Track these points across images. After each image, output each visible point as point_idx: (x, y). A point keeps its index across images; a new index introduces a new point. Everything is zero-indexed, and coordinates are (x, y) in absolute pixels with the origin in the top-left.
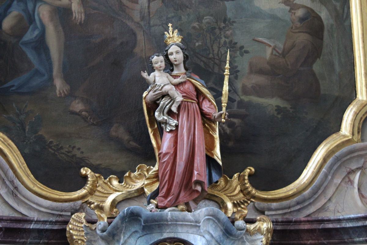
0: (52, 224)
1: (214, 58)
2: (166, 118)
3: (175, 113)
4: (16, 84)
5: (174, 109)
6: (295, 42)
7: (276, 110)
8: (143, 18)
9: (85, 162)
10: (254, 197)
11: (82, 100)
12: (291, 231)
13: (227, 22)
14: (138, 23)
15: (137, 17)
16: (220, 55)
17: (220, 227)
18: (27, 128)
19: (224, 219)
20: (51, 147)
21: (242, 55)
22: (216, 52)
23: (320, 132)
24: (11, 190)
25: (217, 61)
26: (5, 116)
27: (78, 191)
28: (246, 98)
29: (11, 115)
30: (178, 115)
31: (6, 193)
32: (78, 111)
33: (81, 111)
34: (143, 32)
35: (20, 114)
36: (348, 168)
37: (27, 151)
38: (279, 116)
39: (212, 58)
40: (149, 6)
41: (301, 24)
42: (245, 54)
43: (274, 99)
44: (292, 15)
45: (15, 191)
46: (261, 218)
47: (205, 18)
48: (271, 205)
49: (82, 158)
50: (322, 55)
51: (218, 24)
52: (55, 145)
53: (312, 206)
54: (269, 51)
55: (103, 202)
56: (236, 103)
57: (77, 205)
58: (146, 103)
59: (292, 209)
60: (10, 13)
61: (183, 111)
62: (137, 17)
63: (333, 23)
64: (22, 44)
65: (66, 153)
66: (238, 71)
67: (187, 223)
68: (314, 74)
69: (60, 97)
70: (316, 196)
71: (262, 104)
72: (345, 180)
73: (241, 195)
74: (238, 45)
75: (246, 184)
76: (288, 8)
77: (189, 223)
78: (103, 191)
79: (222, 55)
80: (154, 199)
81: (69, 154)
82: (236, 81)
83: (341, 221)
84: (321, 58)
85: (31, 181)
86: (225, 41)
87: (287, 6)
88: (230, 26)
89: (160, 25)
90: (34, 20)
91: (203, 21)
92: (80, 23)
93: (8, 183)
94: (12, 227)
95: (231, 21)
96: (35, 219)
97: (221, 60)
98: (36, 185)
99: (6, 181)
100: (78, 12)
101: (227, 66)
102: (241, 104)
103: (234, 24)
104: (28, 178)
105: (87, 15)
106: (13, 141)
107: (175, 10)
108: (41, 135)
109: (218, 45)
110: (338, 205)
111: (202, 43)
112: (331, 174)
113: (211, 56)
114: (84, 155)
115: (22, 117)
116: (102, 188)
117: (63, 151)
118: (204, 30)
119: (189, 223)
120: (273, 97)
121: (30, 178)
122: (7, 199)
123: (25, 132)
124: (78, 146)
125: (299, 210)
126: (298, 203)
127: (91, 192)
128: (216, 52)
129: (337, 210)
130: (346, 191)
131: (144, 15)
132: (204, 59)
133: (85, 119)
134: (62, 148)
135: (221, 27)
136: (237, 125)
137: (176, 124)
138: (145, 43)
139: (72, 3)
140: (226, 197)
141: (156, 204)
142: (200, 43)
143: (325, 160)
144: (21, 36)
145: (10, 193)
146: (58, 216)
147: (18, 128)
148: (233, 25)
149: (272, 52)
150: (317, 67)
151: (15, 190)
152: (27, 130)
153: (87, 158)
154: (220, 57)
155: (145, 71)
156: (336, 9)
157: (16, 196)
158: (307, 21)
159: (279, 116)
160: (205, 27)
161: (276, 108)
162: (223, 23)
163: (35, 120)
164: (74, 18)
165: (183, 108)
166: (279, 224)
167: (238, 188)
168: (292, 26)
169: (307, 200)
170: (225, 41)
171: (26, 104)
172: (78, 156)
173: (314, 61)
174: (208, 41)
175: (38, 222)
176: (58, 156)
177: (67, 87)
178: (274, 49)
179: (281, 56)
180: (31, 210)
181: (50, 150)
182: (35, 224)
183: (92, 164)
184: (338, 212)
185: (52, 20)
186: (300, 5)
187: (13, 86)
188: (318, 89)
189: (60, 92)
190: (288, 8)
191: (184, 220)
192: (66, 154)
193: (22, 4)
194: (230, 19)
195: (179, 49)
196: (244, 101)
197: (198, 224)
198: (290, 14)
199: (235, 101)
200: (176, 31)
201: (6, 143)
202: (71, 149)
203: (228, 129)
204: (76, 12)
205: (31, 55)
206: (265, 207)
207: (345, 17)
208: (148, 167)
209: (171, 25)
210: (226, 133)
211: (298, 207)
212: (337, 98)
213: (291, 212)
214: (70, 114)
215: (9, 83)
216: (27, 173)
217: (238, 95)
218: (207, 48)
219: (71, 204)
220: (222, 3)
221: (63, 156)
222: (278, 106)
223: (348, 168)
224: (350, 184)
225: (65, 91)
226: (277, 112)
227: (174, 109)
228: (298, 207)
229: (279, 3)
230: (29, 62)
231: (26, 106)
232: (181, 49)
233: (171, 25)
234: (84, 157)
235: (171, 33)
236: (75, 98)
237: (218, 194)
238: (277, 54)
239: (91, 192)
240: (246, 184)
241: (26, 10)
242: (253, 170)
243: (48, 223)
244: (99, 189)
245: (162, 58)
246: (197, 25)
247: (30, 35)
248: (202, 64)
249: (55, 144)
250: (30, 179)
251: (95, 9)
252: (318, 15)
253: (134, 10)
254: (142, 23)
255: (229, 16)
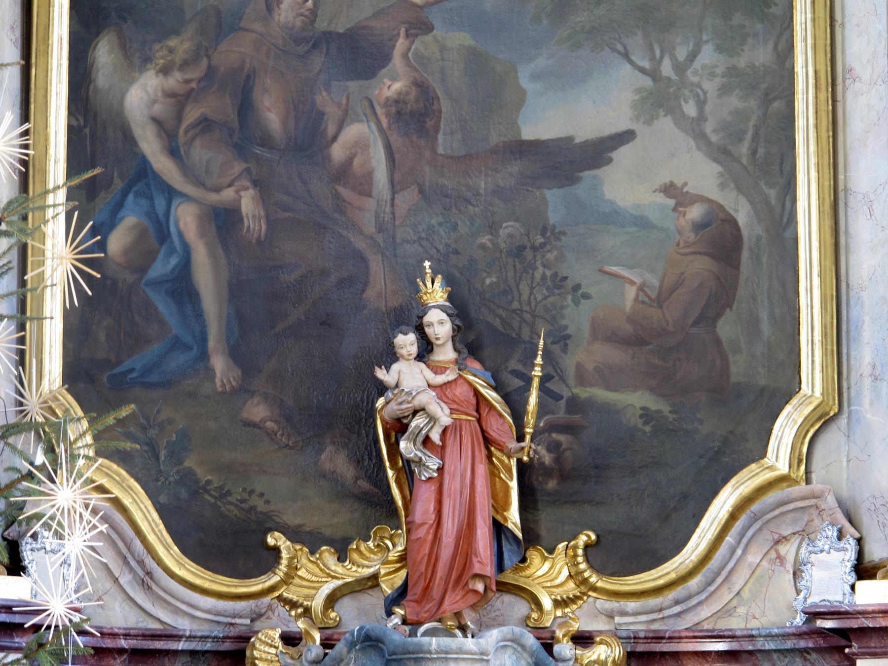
0: (218, 641)
1: (521, 311)
2: (420, 454)
3: (438, 446)
4: (138, 366)
5: (435, 437)
6: (683, 274)
7: (641, 416)
8: (380, 229)
9: (273, 520)
10: (594, 589)
11: (266, 398)
12: (663, 654)
13: (548, 234)
14: (371, 238)
15: (370, 228)
16: (533, 304)
17: (526, 660)
18: (163, 453)
19: (532, 645)
20: (208, 492)
21: (577, 303)
22: (525, 297)
23: (727, 459)
24: (140, 577)
25: (527, 317)
26: (119, 430)
27: (263, 577)
28: (583, 393)
29: (132, 429)
30: (443, 447)
31: (129, 582)
32: (257, 419)
33: (263, 421)
34: (382, 257)
35: (148, 427)
36: (776, 533)
37: (163, 499)
38: (648, 429)
39: (518, 310)
40: (393, 199)
41: (697, 235)
42: (583, 301)
43: (639, 393)
44: (678, 219)
45: (147, 579)
46: (602, 639)
47: (504, 225)
48: (627, 606)
49: (268, 512)
50: (736, 302)
51: (531, 237)
52: (216, 487)
53: (705, 607)
54: (631, 293)
55: (312, 598)
56: (563, 403)
57: (263, 606)
58: (382, 421)
59: (666, 613)
60: (122, 219)
61: (452, 439)
62: (370, 228)
63: (761, 233)
64: (147, 284)
65: (238, 503)
66: (568, 337)
67: (465, 656)
68: (718, 342)
69: (224, 393)
70: (712, 588)
71: (615, 404)
72: (769, 556)
73: (571, 585)
74: (570, 283)
75: (579, 563)
76: (671, 202)
77: (470, 656)
78: (309, 577)
79: (537, 303)
80: (398, 605)
81: (243, 505)
82: (564, 356)
83: (754, 639)
84: (734, 308)
85: (174, 558)
86: (544, 274)
87: (670, 198)
88: (554, 243)
89: (414, 242)
90: (169, 234)
91: (501, 232)
92: (259, 240)
93: (133, 563)
94: (145, 647)
95: (557, 230)
96: (188, 634)
97: (535, 313)
98: (184, 566)
99: (129, 560)
100: (254, 216)
101: (539, 360)
102: (574, 405)
103: (563, 238)
104: (169, 551)
105: (272, 224)
106: (137, 480)
107: (445, 209)
108: (190, 469)
109: (530, 283)
110: (753, 604)
111: (497, 278)
112: (742, 546)
113: (515, 305)
114: (272, 507)
115: (152, 433)
116: (307, 571)
117: (230, 499)
118: (501, 251)
119: (470, 656)
120: (635, 389)
121: (172, 552)
122: (132, 594)
123: (159, 462)
124: (259, 489)
125: (679, 615)
126: (677, 602)
127: (287, 580)
128: (525, 297)
129: (751, 614)
130: (770, 578)
131: (383, 221)
132: (501, 312)
133: (271, 435)
134: (229, 493)
135: (537, 244)
136: (564, 446)
137: (439, 467)
138: (385, 281)
139: (241, 197)
140: (541, 589)
141: (402, 615)
142: (495, 280)
143: (733, 517)
144: (142, 270)
145: (137, 583)
146: (228, 626)
147: (146, 455)
148: (559, 239)
149: (637, 296)
150: (726, 328)
151: (147, 578)
152: (163, 458)
153: (276, 513)
154: (533, 308)
155: (383, 367)
156: (767, 203)
157: (149, 588)
158: (708, 229)
159: (648, 429)
160: (505, 246)
161: (642, 412)
162: (539, 237)
163: (177, 437)
164: (245, 230)
165: (451, 434)
166: (641, 641)
167: (565, 573)
168: (679, 241)
169: (695, 595)
170: (544, 274)
171: (159, 406)
172: (259, 509)
173: (718, 316)
174: (510, 274)
175: (191, 638)
176: (223, 509)
177: (237, 372)
178: (641, 289)
179: (655, 304)
180: (177, 614)
181: (207, 497)
182: (186, 641)
183: (287, 524)
184: (754, 617)
185: (202, 234)
186: (697, 195)
187: (132, 370)
188: (725, 372)
189: (222, 382)
190: (671, 202)
191: (460, 651)
192: (236, 506)
193: (143, 202)
194: (554, 226)
195: (444, 316)
196: (579, 397)
197: (485, 658)
198: (675, 215)
199: (562, 397)
200: (439, 280)
201: (124, 485)
202: (246, 496)
203: (546, 454)
204: (250, 216)
205: (164, 306)
206: (615, 609)
207: (785, 220)
208: (393, 532)
209: (430, 263)
210: (543, 463)
211: (677, 609)
212: (763, 390)
213: (663, 618)
214: (242, 426)
215: (125, 364)
216: (167, 543)
217: (567, 386)
218: (507, 288)
219: (251, 603)
220: (538, 194)
221: (232, 508)
222: (644, 408)
223: (776, 533)
224: (779, 564)
225: (231, 379)
226: (642, 421)
227: (435, 437)
228: (677, 609)
229: (654, 192)
230: (162, 323)
231: (158, 412)
232: (448, 315)
233: (430, 263)
234: (272, 511)
235: (429, 284)
236: (253, 393)
237: (525, 584)
238: (646, 299)
239: (287, 580)
240: (579, 563)
241: (151, 214)
242: (593, 537)
243: (210, 640)
244: (300, 573)
245: (412, 337)
246: (488, 240)
247: (161, 267)
248: (497, 323)
249: (216, 485)
250: (172, 555)
251: (286, 209)
252: (733, 217)
253: (363, 209)
254: (380, 238)
255: (551, 222)
